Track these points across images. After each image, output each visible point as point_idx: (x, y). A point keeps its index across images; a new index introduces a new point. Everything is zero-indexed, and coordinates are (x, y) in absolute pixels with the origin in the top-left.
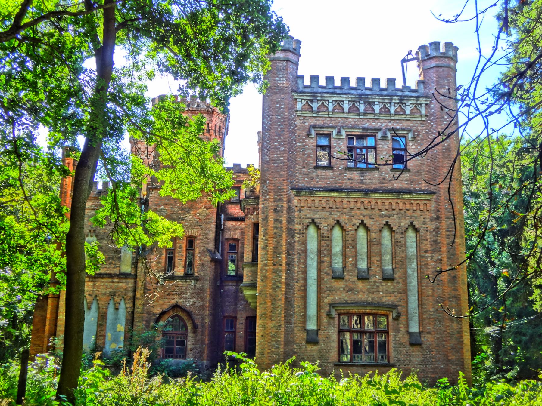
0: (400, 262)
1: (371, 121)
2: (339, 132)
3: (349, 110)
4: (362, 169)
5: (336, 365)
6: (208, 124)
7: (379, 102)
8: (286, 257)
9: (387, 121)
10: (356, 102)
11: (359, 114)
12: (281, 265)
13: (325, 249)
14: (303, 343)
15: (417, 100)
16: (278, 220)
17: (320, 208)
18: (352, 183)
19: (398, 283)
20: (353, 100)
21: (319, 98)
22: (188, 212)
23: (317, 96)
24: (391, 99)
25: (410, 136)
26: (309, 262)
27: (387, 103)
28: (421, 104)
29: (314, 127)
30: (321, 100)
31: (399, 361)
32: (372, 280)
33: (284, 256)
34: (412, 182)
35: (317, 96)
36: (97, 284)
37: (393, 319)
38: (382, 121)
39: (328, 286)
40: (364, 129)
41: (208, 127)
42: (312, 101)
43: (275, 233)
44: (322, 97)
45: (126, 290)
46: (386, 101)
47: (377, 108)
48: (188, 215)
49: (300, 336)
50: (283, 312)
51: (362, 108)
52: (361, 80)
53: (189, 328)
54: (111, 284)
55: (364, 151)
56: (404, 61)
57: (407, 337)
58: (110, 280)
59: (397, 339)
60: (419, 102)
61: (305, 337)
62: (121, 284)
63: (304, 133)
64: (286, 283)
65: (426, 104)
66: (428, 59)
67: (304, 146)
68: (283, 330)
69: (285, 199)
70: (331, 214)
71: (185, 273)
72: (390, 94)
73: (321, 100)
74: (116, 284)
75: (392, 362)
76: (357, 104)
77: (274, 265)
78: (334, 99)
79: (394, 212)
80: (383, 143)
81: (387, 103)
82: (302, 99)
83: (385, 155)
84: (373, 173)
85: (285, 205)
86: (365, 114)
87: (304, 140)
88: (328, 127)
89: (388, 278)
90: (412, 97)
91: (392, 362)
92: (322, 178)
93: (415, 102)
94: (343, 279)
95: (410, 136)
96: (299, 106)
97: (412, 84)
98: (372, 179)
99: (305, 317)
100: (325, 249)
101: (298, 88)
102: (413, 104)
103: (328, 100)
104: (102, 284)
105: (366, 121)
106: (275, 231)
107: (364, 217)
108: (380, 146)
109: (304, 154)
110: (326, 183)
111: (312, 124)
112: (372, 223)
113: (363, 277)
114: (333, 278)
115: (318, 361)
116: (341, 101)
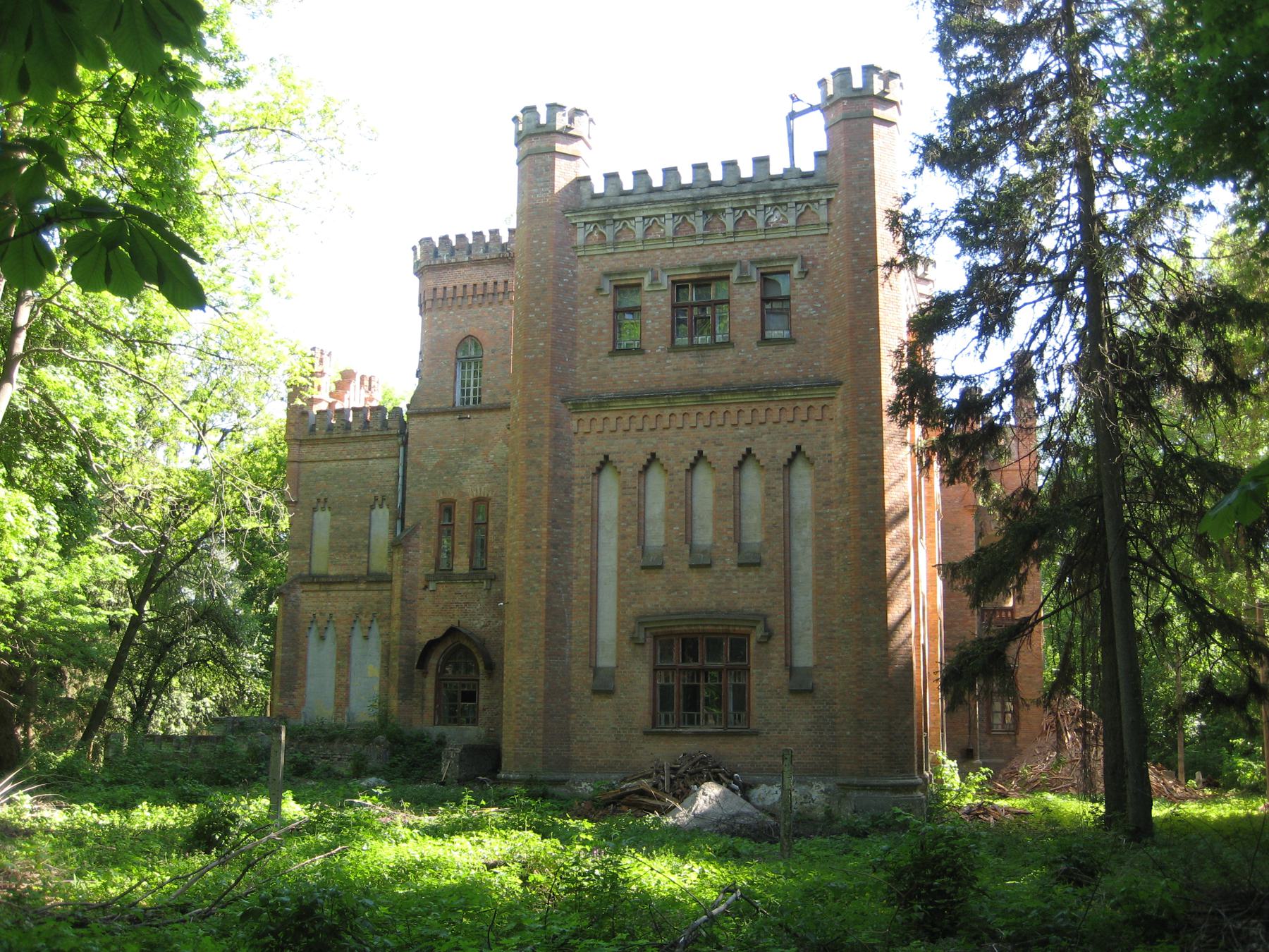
0: (785, 525)
1: (719, 248)
2: (655, 279)
3: (675, 232)
4: (701, 347)
5: (646, 733)
6: (506, 282)
7: (734, 209)
8: (549, 532)
9: (751, 245)
10: (687, 213)
11: (693, 237)
12: (539, 547)
13: (635, 511)
14: (588, 692)
15: (809, 194)
16: (533, 462)
17: (620, 433)
18: (680, 378)
19: (769, 570)
20: (682, 211)
21: (616, 217)
22: (474, 453)
23: (613, 213)
24: (756, 199)
25: (796, 269)
26: (603, 538)
27: (748, 208)
28: (818, 201)
29: (607, 275)
30: (620, 220)
31: (767, 724)
32: (717, 568)
33: (545, 530)
34: (800, 364)
35: (613, 213)
36: (333, 594)
37: (759, 643)
38: (740, 246)
39: (633, 582)
40: (703, 266)
41: (506, 288)
42: (602, 223)
43: (529, 488)
44: (621, 213)
45: (378, 602)
46: (747, 204)
47: (729, 221)
48: (474, 459)
49: (580, 677)
50: (542, 636)
51: (699, 223)
52: (730, 166)
53: (481, 668)
54: (354, 593)
55: (708, 311)
56: (792, 115)
57: (784, 675)
58: (353, 587)
59: (765, 681)
60: (813, 198)
61: (590, 681)
62: (370, 594)
63: (592, 289)
64: (547, 582)
65: (829, 201)
66: (832, 105)
67: (591, 314)
68: (542, 668)
69: (547, 421)
70: (639, 443)
71: (472, 568)
72: (758, 193)
73: (620, 220)
74: (363, 594)
75: (754, 726)
76: (690, 219)
77: (528, 548)
78: (645, 214)
79: (764, 428)
80: (743, 290)
81: (748, 208)
82: (586, 223)
83: (747, 314)
84: (722, 352)
85: (547, 432)
86: (704, 235)
87: (590, 302)
88: (633, 272)
89: (750, 563)
90: (798, 188)
91: (754, 726)
92: (626, 373)
93: (805, 198)
94: (661, 567)
95: (796, 269)
96: (580, 237)
97: (806, 164)
98: (722, 366)
99: (593, 642)
100: (635, 511)
101: (581, 203)
102: (802, 203)
103: (633, 218)
104: (341, 594)
105: (710, 249)
106: (529, 483)
107: (703, 442)
108: (737, 297)
109: (590, 330)
110: (631, 382)
111: (606, 269)
112: (719, 454)
113: (702, 565)
114: (643, 568)
115: (70, 752)
116: (658, 216)
